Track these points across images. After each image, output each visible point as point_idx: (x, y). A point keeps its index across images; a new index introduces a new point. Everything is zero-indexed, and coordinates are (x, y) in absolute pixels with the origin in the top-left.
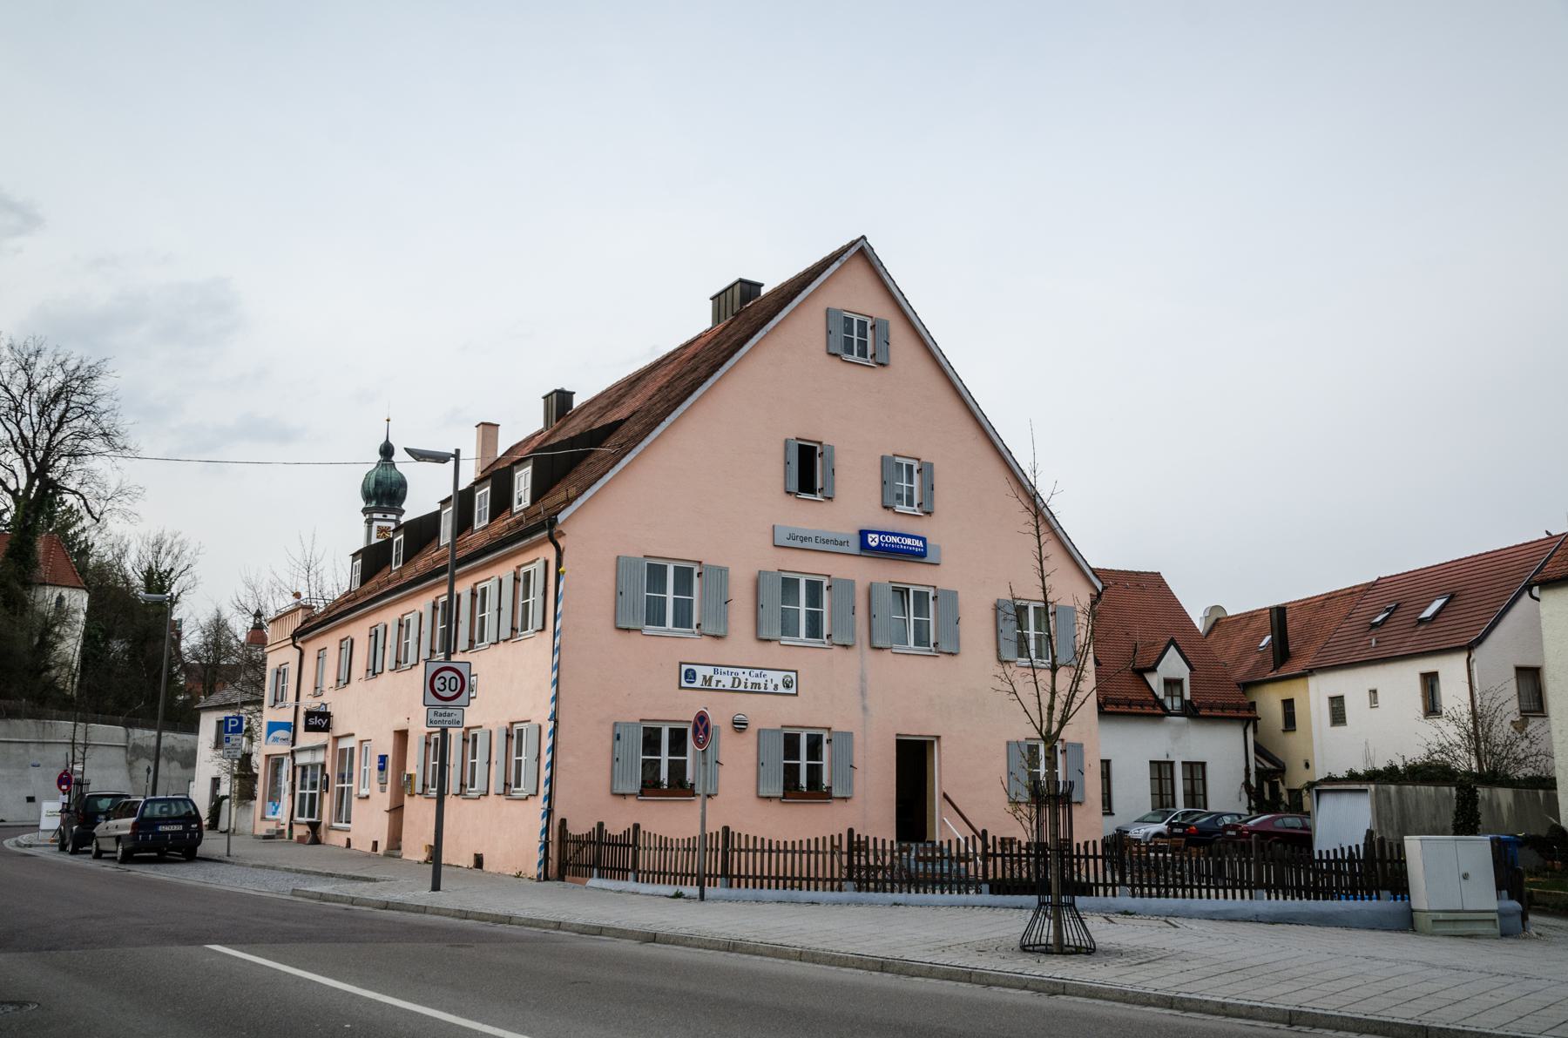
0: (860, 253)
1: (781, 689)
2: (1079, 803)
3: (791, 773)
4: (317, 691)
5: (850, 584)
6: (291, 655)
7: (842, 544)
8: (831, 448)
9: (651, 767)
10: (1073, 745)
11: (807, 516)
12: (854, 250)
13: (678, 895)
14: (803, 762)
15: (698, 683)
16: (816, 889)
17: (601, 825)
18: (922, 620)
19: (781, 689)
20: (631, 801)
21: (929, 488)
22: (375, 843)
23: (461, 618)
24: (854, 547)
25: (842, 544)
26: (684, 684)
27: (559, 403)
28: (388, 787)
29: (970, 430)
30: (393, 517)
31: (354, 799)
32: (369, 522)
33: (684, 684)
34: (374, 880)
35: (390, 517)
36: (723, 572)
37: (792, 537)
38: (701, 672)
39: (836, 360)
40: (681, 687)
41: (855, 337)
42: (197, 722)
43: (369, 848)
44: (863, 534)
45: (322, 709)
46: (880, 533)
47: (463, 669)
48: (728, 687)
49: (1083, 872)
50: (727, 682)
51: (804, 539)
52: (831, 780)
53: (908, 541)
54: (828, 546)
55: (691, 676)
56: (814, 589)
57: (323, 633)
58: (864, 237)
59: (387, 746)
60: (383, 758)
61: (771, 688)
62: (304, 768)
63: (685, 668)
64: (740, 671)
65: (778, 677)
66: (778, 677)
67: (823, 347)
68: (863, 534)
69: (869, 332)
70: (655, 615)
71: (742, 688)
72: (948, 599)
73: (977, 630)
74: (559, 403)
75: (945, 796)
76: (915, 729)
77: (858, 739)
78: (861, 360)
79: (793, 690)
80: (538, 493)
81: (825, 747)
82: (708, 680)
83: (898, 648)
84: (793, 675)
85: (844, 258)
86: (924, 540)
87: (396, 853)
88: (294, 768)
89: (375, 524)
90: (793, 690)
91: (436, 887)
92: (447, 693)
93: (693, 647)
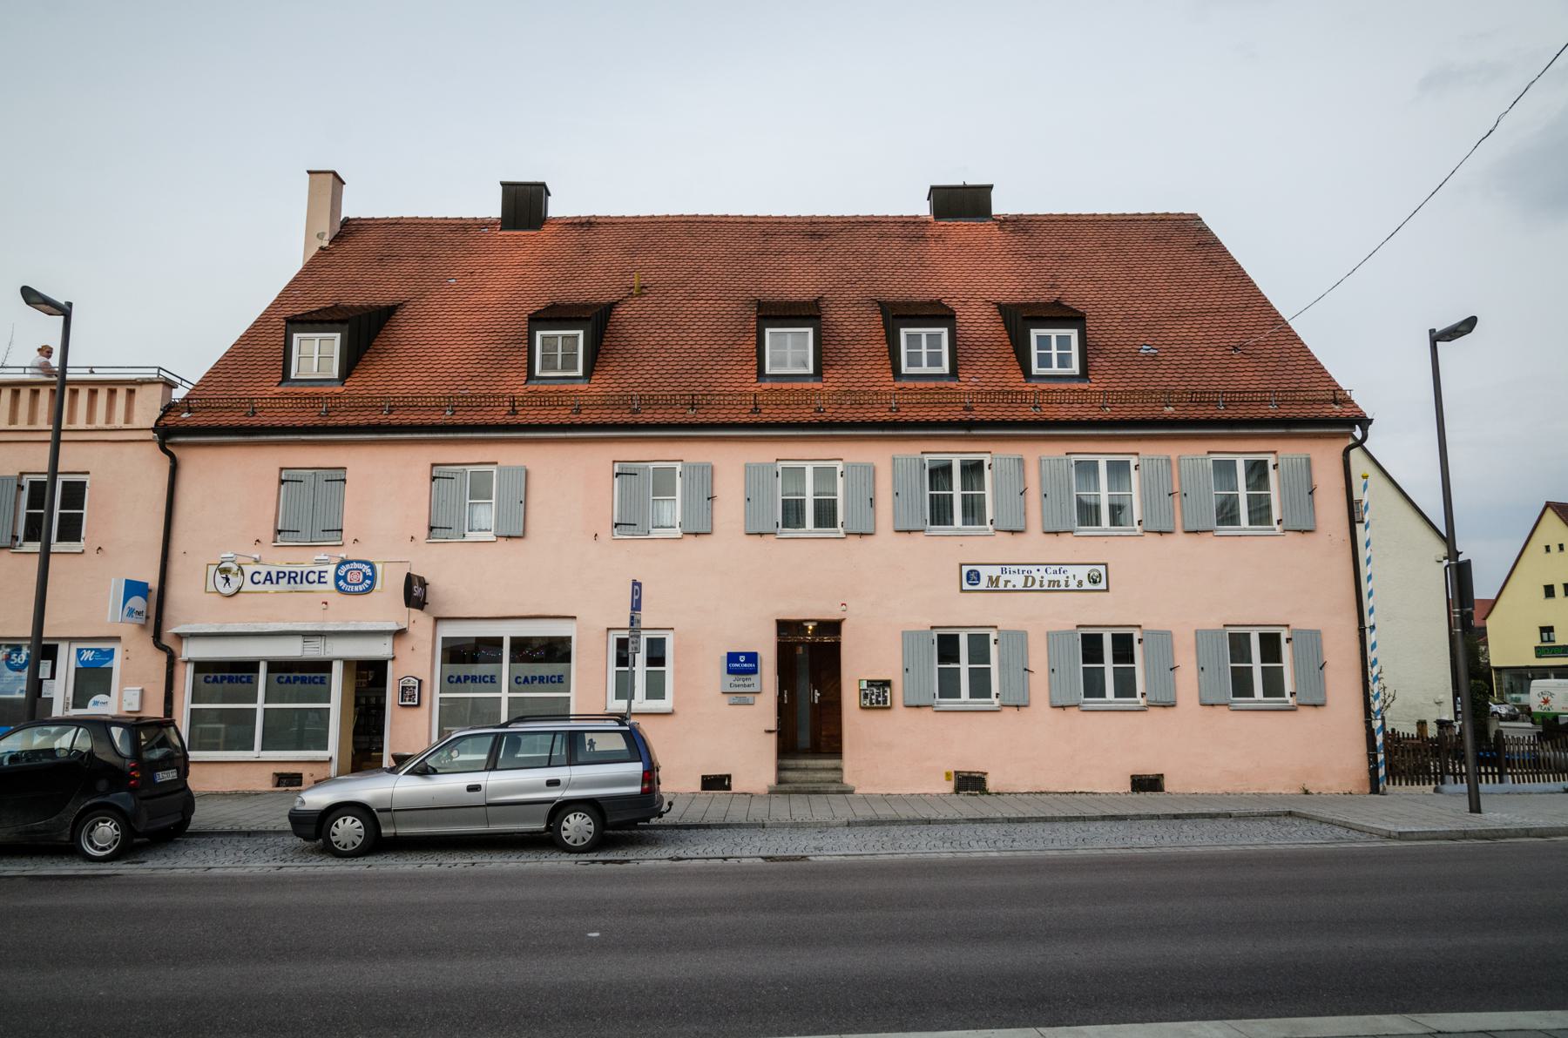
1: (1087, 585)
2: (770, 732)
10: (1154, 633)
15: (983, 584)
26: (966, 586)
33: (1103, 586)
38: (985, 572)
40: (962, 590)
42: (906, 652)
48: (1020, 586)
50: (1018, 581)
55: (973, 577)
63: (966, 569)
66: (1082, 573)
70: (940, 513)
71: (1037, 586)
76: (1550, 600)
79: (1103, 586)
82: (993, 581)
91: (1475, 808)
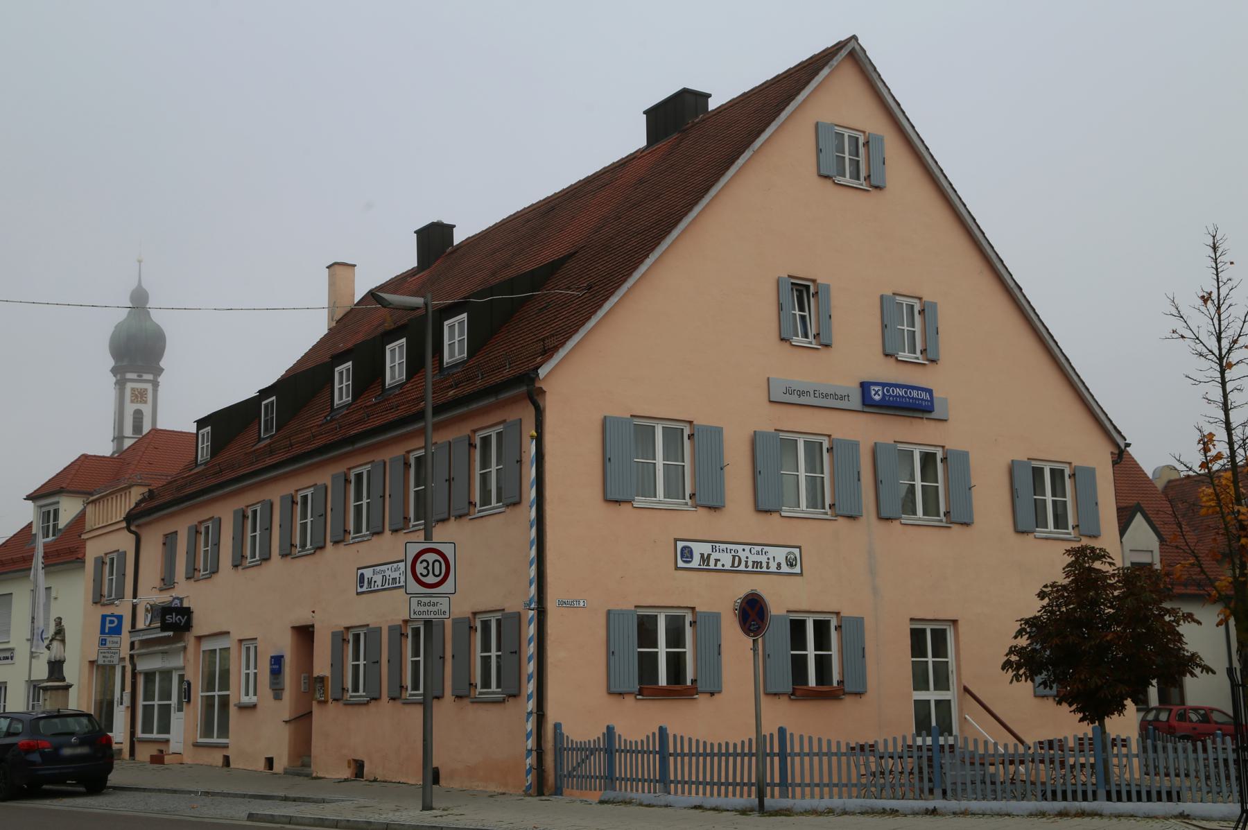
0: (848, 55)
1: (785, 568)
3: (647, 664)
4: (167, 582)
5: (854, 445)
6: (124, 542)
7: (842, 398)
8: (827, 287)
9: (647, 664)
11: (803, 369)
12: (844, 53)
13: (934, 812)
14: (662, 650)
15: (695, 563)
16: (812, 796)
17: (610, 730)
18: (931, 491)
19: (785, 568)
20: (629, 700)
21: (931, 331)
22: (270, 762)
23: (862, 473)
24: (856, 402)
25: (842, 398)
26: (681, 564)
27: (434, 239)
28: (287, 695)
29: (972, 261)
30: (150, 377)
31: (233, 710)
32: (121, 384)
33: (681, 564)
34: (324, 801)
35: (146, 377)
36: (716, 433)
37: (789, 391)
38: (699, 549)
39: (829, 182)
40: (677, 568)
41: (847, 156)
43: (261, 765)
44: (865, 386)
45: (177, 603)
46: (883, 385)
47: (447, 550)
48: (728, 567)
49: (844, 766)
50: (726, 560)
51: (802, 393)
52: (842, 673)
53: (915, 394)
54: (826, 402)
55: (687, 554)
56: (814, 450)
57: (172, 515)
58: (854, 38)
59: (285, 644)
60: (277, 661)
61: (773, 568)
62: (149, 676)
63: (680, 545)
64: (740, 548)
65: (780, 554)
66: (780, 554)
67: (814, 169)
68: (865, 386)
69: (862, 150)
71: (742, 567)
72: (957, 461)
73: (991, 499)
74: (434, 239)
75: (966, 690)
77: (869, 625)
78: (854, 183)
79: (797, 570)
80: (475, 345)
81: (834, 635)
82: (705, 559)
83: (906, 519)
84: (796, 551)
85: (834, 62)
86: (930, 391)
87: (306, 770)
88: (134, 675)
89: (129, 386)
90: (797, 570)
92: (431, 579)
93: (694, 522)
